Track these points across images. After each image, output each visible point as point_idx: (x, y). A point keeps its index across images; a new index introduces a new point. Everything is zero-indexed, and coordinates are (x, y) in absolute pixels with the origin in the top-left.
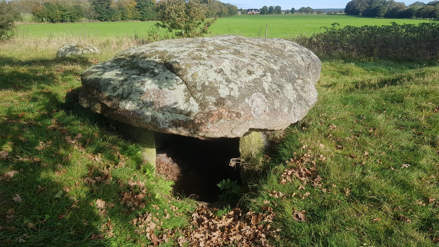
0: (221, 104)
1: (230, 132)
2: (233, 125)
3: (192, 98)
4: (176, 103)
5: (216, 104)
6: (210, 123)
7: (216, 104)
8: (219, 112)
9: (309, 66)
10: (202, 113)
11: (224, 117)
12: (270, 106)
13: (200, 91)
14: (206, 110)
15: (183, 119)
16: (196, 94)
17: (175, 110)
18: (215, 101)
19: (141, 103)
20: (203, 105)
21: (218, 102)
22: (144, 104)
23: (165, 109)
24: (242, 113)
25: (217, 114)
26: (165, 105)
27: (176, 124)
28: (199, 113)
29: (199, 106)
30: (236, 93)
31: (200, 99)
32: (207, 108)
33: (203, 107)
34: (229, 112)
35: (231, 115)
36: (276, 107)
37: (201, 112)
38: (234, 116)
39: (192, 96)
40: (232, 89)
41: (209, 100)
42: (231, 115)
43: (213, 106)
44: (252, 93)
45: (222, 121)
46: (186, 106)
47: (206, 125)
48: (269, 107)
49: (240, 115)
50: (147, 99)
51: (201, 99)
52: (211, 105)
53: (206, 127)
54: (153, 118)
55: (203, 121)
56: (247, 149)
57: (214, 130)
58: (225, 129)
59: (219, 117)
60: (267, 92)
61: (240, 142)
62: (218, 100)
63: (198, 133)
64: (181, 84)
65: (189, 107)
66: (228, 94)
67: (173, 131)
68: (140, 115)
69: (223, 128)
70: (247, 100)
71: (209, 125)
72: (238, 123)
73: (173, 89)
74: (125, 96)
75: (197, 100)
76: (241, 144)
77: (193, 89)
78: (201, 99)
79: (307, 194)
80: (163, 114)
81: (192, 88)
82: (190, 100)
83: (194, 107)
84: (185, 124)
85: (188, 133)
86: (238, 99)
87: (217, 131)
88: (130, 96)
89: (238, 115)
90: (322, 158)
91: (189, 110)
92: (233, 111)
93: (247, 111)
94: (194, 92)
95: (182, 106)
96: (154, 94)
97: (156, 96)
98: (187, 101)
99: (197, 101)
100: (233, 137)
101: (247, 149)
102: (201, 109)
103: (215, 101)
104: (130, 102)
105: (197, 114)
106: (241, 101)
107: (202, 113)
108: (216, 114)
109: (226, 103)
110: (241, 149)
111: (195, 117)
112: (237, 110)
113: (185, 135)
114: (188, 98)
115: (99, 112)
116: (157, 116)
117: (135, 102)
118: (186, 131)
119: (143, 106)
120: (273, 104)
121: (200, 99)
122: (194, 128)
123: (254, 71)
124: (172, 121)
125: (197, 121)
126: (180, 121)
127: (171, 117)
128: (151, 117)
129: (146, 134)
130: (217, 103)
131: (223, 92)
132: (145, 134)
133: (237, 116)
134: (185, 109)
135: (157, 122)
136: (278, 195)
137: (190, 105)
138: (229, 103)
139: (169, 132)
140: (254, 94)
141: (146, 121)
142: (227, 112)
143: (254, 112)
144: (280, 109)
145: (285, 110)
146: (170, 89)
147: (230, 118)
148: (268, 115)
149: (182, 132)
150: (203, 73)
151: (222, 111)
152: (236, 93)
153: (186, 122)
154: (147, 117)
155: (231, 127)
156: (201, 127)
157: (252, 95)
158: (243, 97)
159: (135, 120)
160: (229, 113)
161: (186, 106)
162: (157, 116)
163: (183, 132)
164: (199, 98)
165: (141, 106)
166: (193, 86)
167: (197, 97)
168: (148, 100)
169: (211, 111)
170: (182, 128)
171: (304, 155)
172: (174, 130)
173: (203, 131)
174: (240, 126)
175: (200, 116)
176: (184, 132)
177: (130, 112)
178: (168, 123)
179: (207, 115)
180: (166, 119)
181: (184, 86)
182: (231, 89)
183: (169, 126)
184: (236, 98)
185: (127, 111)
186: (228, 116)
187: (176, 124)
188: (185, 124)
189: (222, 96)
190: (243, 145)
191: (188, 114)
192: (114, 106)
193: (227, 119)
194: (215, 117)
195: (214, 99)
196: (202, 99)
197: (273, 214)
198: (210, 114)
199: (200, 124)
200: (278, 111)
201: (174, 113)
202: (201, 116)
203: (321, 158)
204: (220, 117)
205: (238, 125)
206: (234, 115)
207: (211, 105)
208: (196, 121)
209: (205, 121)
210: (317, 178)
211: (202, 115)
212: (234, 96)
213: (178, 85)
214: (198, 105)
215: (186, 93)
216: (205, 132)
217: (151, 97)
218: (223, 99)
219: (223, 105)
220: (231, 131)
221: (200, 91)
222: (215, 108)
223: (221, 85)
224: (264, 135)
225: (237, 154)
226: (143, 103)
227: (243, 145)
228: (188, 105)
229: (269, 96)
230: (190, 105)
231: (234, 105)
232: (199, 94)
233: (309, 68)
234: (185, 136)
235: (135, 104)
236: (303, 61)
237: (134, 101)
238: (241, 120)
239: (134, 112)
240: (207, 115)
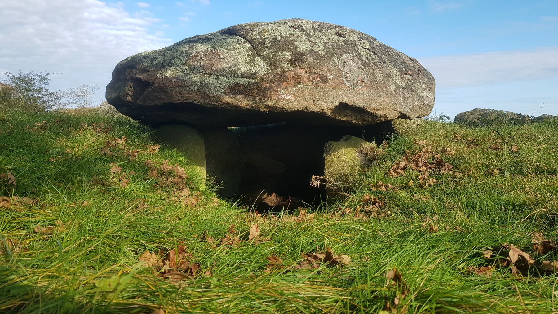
0: (299, 62)
1: (312, 102)
2: (316, 92)
3: (257, 58)
4: (235, 66)
5: (292, 62)
6: (283, 89)
7: (292, 62)
8: (296, 74)
9: (419, 72)
10: (272, 74)
11: (304, 80)
12: (369, 75)
13: (270, 47)
14: (278, 69)
15: (244, 83)
16: (264, 52)
17: (233, 73)
18: (290, 57)
19: (186, 69)
20: (273, 64)
21: (295, 58)
22: (191, 69)
23: (219, 73)
24: (330, 77)
25: (293, 77)
26: (220, 67)
27: (234, 90)
28: (267, 73)
29: (267, 66)
30: (320, 49)
31: (269, 57)
32: (279, 67)
33: (273, 67)
34: (311, 73)
35: (314, 79)
36: (377, 79)
37: (270, 73)
38: (318, 81)
39: (258, 55)
40: (315, 43)
41: (282, 57)
42: (314, 79)
43: (287, 65)
44: (343, 53)
45: (300, 86)
46: (249, 67)
47: (277, 90)
48: (368, 76)
49: (327, 79)
50: (196, 62)
51: (270, 56)
52: (284, 63)
53: (277, 94)
54: (203, 84)
55: (274, 85)
56: (336, 169)
57: (289, 97)
58: (305, 97)
59: (296, 82)
60: (365, 59)
61: (326, 162)
62: (295, 55)
63: (266, 101)
64: (244, 43)
65: (253, 68)
66: (309, 48)
67: (229, 99)
68: (184, 81)
69: (301, 96)
70: (336, 60)
71: (282, 91)
72: (323, 90)
73: (233, 49)
74: (166, 63)
75: (265, 59)
76: (327, 165)
77: (260, 47)
78: (270, 56)
79: (432, 181)
80: (217, 79)
81: (258, 45)
82: (256, 59)
83: (261, 67)
84: (246, 91)
85: (251, 103)
86: (324, 56)
87: (293, 98)
88: (173, 61)
89: (324, 79)
90: (449, 152)
91: (253, 71)
92: (316, 71)
93: (336, 75)
94: (261, 49)
95: (244, 68)
96: (206, 56)
97: (208, 58)
98: (251, 61)
99: (265, 61)
100: (316, 109)
101: (336, 169)
102: (270, 69)
103: (290, 57)
104: (172, 68)
105: (265, 75)
106: (328, 59)
107: (272, 73)
108: (291, 77)
109: (306, 60)
110: (327, 171)
111: (262, 79)
112: (322, 71)
113: (246, 107)
114: (252, 58)
115: (129, 99)
116: (208, 81)
117: (178, 68)
118: (249, 100)
119: (190, 73)
120: (373, 74)
121: (269, 57)
122: (260, 95)
123: (345, 34)
124: (229, 86)
125: (265, 85)
126: (241, 84)
127: (226, 82)
128: (199, 83)
129: (194, 150)
130: (294, 60)
131: (303, 46)
132: (193, 149)
133: (322, 81)
134: (248, 71)
135: (208, 88)
136: (386, 187)
137: (255, 66)
138: (311, 60)
139: (224, 101)
140: (345, 54)
141: (192, 88)
142: (308, 74)
143: (347, 78)
144: (384, 83)
145: (391, 87)
146: (228, 49)
147: (312, 82)
148: (366, 86)
149: (242, 102)
150: (275, 30)
151: (300, 72)
152: (320, 49)
153: (249, 86)
154: (195, 82)
155: (313, 94)
156: (269, 92)
157: (342, 54)
158: (330, 55)
159: (178, 89)
160: (310, 75)
161: (249, 67)
162: (208, 81)
163: (244, 101)
164: (268, 55)
165: (186, 72)
166: (260, 43)
167: (265, 55)
168: (197, 63)
169: (284, 72)
170: (243, 96)
171: (423, 150)
172: (231, 98)
173: (272, 98)
174: (327, 95)
175: (269, 77)
176: (244, 102)
177: (172, 79)
178: (223, 89)
179: (278, 77)
180: (220, 84)
181: (247, 45)
182: (314, 42)
183: (225, 93)
184: (320, 54)
185: (168, 78)
186: (308, 78)
187: (234, 90)
188: (246, 91)
189: (300, 50)
190: (330, 165)
191: (252, 76)
192: (150, 77)
193: (307, 83)
194: (290, 81)
195: (289, 55)
196: (272, 57)
197: (379, 204)
198: (282, 77)
199: (269, 88)
200: (380, 84)
201: (232, 77)
202: (270, 78)
203: (448, 152)
204: (298, 80)
205: (323, 92)
206: (318, 79)
207: (284, 63)
208: (263, 84)
209: (276, 86)
210: (445, 166)
211: (272, 76)
212: (317, 52)
213: (239, 44)
214: (266, 64)
215: (250, 53)
216: (275, 99)
217: (201, 59)
218: (302, 54)
219: (302, 63)
220: (314, 100)
221: (270, 47)
222: (291, 68)
223: (299, 39)
224: (361, 154)
225: (321, 172)
226: (191, 68)
227: (330, 165)
228: (252, 66)
229: (367, 64)
230: (255, 66)
231: (317, 64)
232: (268, 51)
233: (419, 74)
234: (247, 108)
235: (178, 70)
236: (411, 61)
237: (178, 66)
238: (328, 86)
239: (177, 78)
240: (278, 77)
